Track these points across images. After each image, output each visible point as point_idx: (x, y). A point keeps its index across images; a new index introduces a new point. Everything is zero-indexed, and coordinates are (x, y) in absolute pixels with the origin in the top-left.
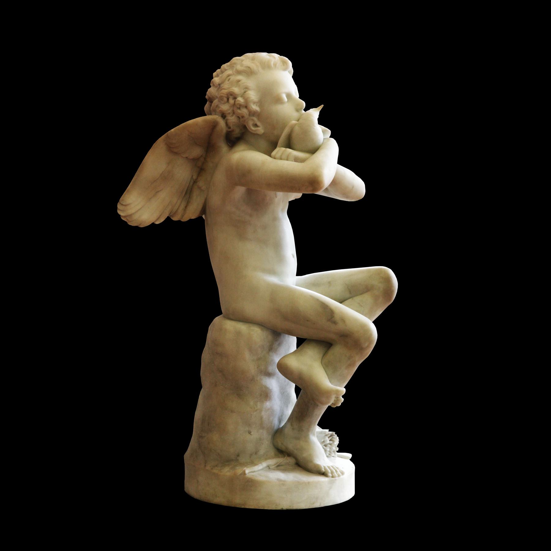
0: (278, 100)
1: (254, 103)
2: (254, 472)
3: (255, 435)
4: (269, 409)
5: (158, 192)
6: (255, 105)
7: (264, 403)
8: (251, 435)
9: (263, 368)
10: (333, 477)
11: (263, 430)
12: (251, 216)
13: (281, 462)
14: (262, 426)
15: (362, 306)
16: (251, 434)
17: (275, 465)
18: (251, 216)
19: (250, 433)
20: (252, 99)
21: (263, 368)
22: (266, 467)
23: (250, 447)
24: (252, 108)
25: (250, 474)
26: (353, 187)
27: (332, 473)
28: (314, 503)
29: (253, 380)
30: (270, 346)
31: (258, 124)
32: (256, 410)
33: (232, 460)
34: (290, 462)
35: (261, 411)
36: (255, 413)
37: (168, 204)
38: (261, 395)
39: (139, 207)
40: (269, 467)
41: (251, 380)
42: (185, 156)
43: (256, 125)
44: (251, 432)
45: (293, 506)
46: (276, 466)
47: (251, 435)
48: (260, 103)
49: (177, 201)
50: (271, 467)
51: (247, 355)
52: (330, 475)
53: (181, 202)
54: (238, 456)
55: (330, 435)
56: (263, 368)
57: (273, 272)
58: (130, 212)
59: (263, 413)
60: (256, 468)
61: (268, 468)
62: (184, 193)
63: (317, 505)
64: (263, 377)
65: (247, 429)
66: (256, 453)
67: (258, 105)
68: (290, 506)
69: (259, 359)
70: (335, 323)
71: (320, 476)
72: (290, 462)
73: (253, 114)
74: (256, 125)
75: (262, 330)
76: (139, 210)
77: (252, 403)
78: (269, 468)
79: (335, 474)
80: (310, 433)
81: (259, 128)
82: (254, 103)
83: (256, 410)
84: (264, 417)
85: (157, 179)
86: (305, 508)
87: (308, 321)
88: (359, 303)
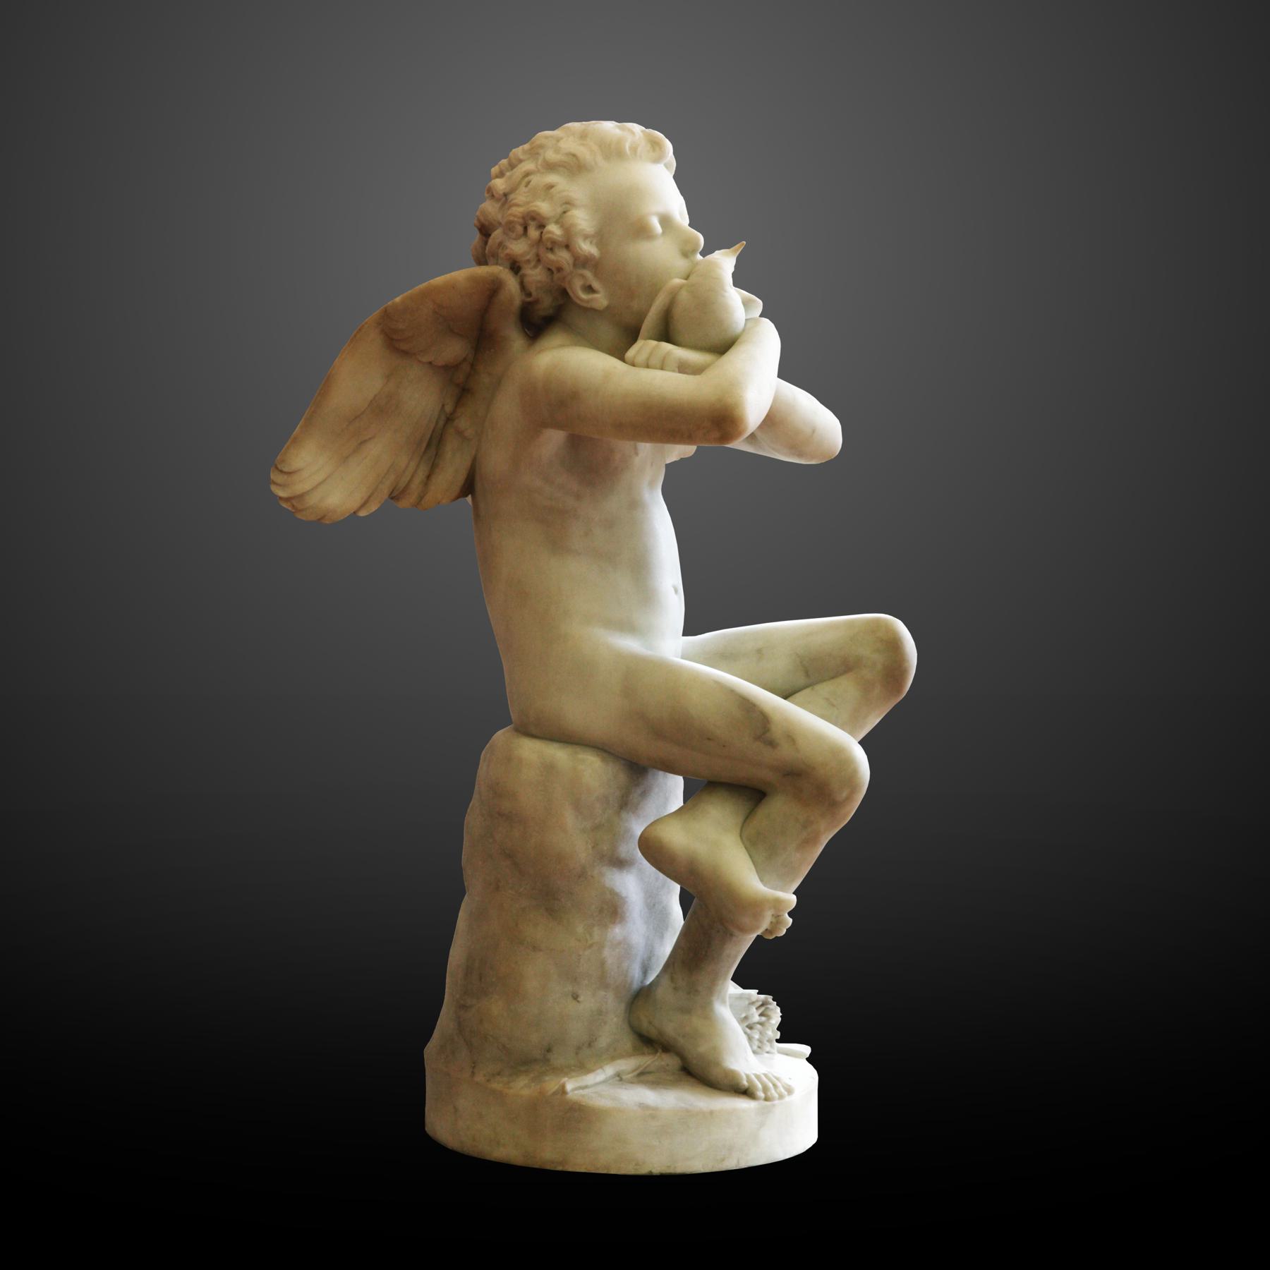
0: (641, 231)
1: (586, 237)
2: (586, 1087)
3: (588, 1002)
4: (620, 943)
5: (364, 442)
6: (588, 242)
7: (609, 930)
8: (578, 1002)
9: (605, 848)
10: (766, 1099)
11: (606, 992)
12: (578, 497)
13: (649, 1065)
14: (603, 982)
15: (833, 706)
16: (579, 999)
17: (633, 1071)
18: (578, 497)
19: (575, 997)
20: (580, 227)
21: (605, 847)
22: (612, 1077)
23: (576, 1031)
24: (581, 249)
25: (576, 1092)
26: (814, 431)
27: (765, 1089)
28: (723, 1160)
29: (583, 875)
30: (623, 796)
31: (596, 285)
32: (591, 946)
33: (536, 1061)
34: (668, 1065)
35: (601, 946)
36: (587, 953)
37: (388, 471)
38: (601, 911)
39: (320, 477)
40: (619, 1077)
41: (579, 877)
42: (425, 359)
43: (590, 289)
44: (577, 996)
45: (675, 1167)
46: (636, 1073)
47: (578, 1002)
48: (600, 237)
49: (409, 463)
50: (624, 1077)
51: (569, 818)
52: (761, 1094)
53: (418, 466)
54: (549, 1050)
55: (760, 1003)
56: (605, 848)
57: (628, 627)
58: (299, 488)
59: (606, 952)
60: (591, 1079)
61: (618, 1078)
62: (424, 445)
63: (732, 1164)
64: (605, 869)
65: (570, 988)
66: (590, 1045)
67: (594, 241)
68: (669, 1167)
69: (596, 828)
70: (772, 744)
71: (738, 1097)
72: (668, 1065)
73: (582, 262)
74: (590, 289)
75: (603, 760)
76: (319, 484)
77: (580, 929)
78: (621, 1080)
79: (773, 1092)
80: (714, 998)
81: (596, 296)
82: (586, 237)
83: (591, 946)
84: (609, 961)
85: (363, 413)
86: (702, 1171)
87: (709, 739)
88: (827, 699)
